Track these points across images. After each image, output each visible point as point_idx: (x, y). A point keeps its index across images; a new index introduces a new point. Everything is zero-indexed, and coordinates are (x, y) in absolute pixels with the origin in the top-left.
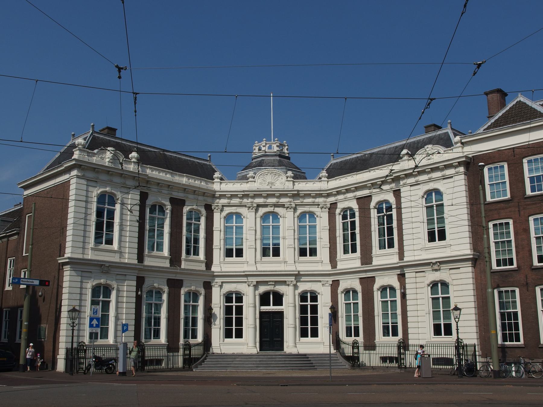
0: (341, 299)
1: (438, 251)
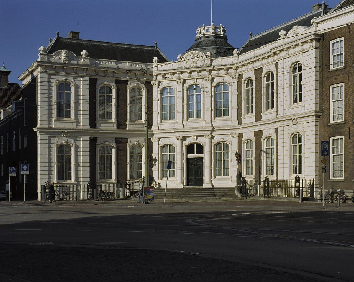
0: (244, 146)
1: (68, 124)
